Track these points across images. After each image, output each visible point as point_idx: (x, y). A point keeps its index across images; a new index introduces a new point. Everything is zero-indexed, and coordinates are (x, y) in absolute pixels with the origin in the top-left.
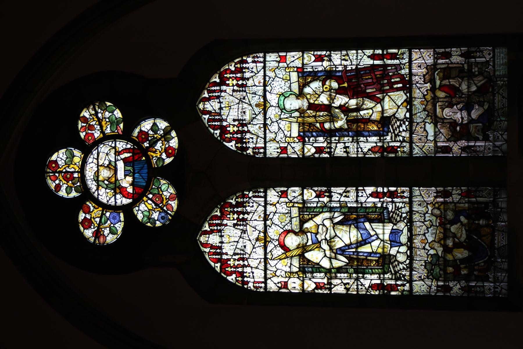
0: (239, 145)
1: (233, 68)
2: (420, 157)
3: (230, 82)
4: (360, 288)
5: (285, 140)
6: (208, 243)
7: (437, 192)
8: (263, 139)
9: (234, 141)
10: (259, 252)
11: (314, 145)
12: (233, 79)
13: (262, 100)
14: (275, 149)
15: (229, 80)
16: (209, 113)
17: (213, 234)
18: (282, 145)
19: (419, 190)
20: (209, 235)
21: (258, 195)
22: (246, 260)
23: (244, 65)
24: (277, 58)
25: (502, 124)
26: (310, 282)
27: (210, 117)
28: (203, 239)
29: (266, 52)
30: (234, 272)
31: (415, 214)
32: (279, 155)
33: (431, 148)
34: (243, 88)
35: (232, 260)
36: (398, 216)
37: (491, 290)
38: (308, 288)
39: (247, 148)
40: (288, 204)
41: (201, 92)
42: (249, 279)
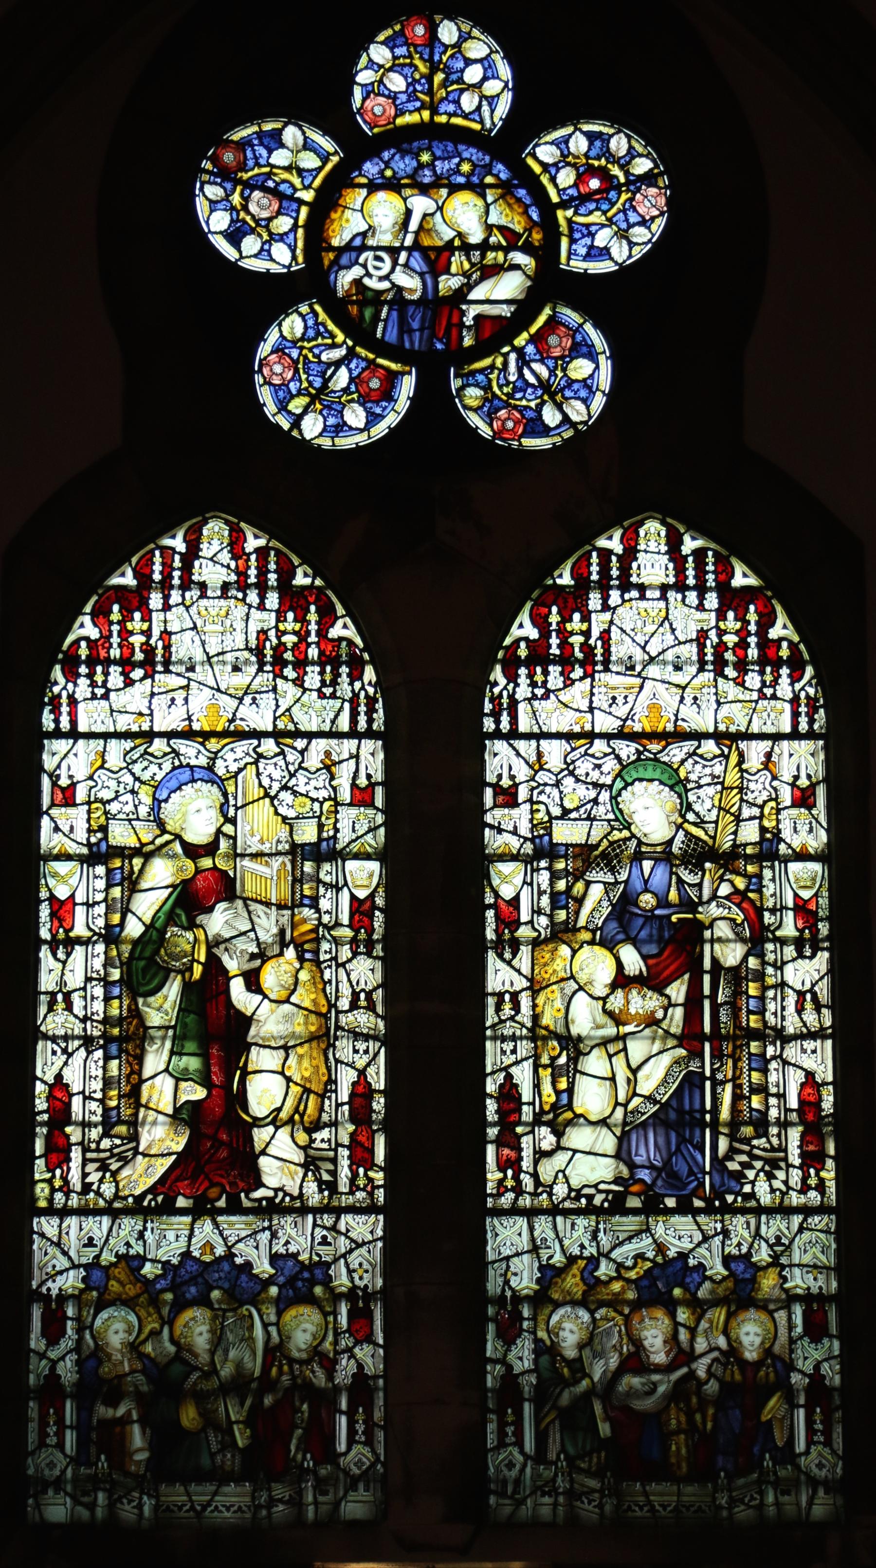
0: (523, 652)
1: (774, 633)
3: (731, 623)
4: (505, 1046)
9: (330, 636)
12: (743, 633)
14: (510, 768)
15: (736, 619)
16: (630, 553)
17: (671, 566)
19: (375, 1240)
20: (666, 553)
21: (799, 714)
22: (585, 672)
23: (344, 670)
24: (809, 777)
25: (590, 1508)
26: (519, 880)
27: (614, 559)
30: (545, 633)
31: (748, 1227)
34: (713, 663)
36: (740, 1163)
38: (55, 875)
39: (72, 675)
41: (262, 526)
42: (523, 680)
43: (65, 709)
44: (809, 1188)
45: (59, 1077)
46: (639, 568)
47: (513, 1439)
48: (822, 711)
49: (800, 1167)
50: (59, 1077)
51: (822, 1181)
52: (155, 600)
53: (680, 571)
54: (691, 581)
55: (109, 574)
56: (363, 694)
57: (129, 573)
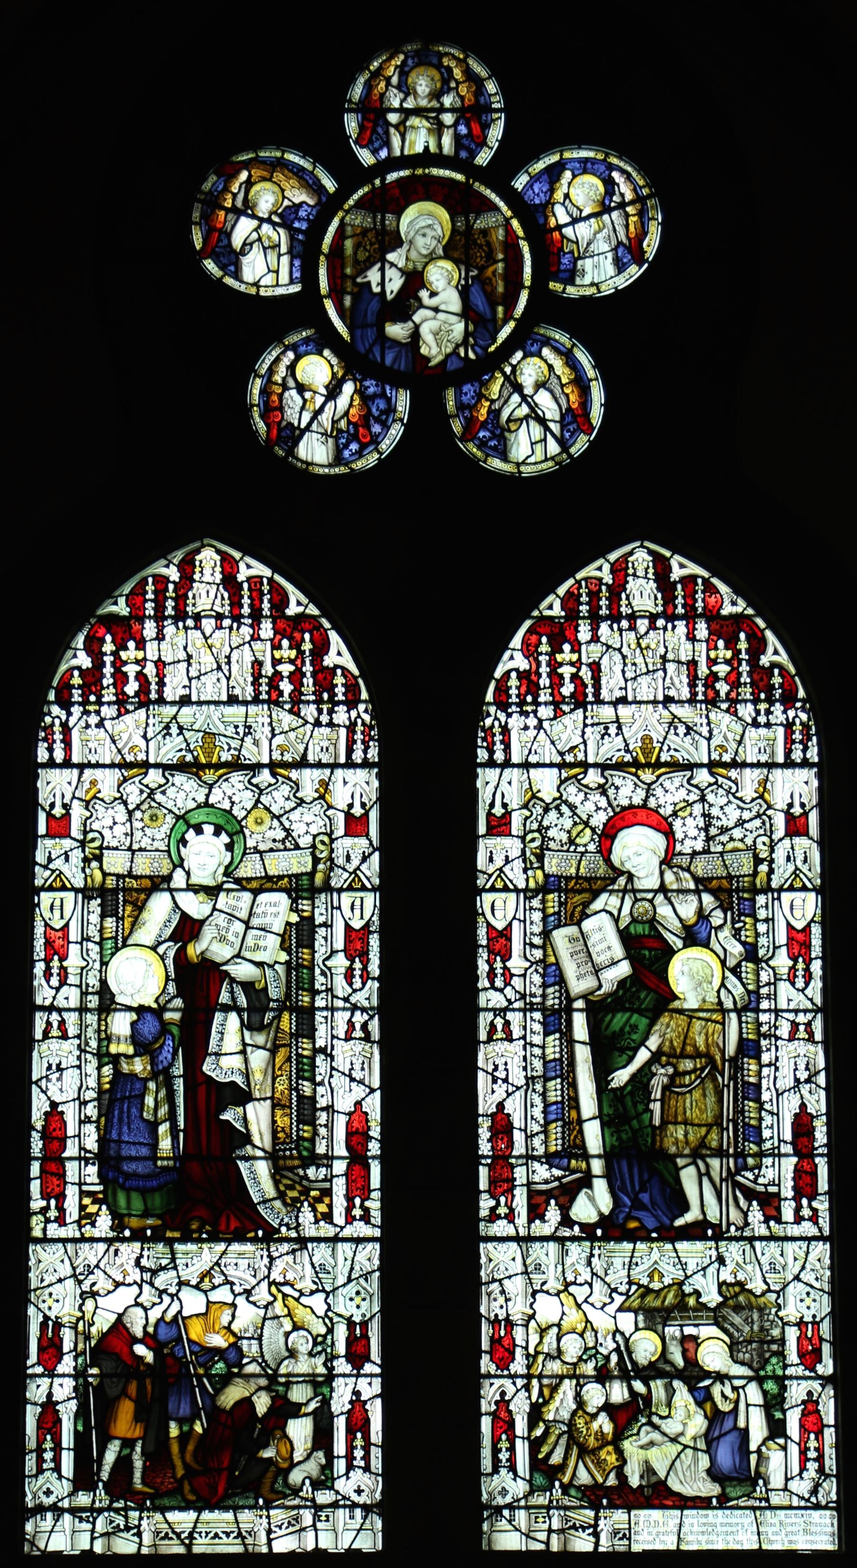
0: (77, 680)
2: (479, 1267)
5: (92, 831)
6: (630, 579)
7: (816, 1324)
8: (734, 760)
9: (325, 663)
10: (169, 746)
11: (515, 924)
13: (226, 757)
15: (727, 648)
17: (659, 595)
18: (516, 820)
21: (355, 742)
28: (208, 558)
29: (824, 770)
32: (43, 809)
33: (55, 1306)
35: (140, 655)
37: (504, 1496)
39: (66, 704)
40: (766, 839)
43: (498, 738)
44: (802, 1219)
45: (501, 1106)
46: (628, 598)
47: (52, 1465)
48: (814, 739)
49: (794, 1198)
50: (501, 1106)
51: (815, 1211)
52: (149, 629)
53: (236, 603)
54: (246, 610)
55: (99, 604)
56: (359, 721)
57: (122, 601)
